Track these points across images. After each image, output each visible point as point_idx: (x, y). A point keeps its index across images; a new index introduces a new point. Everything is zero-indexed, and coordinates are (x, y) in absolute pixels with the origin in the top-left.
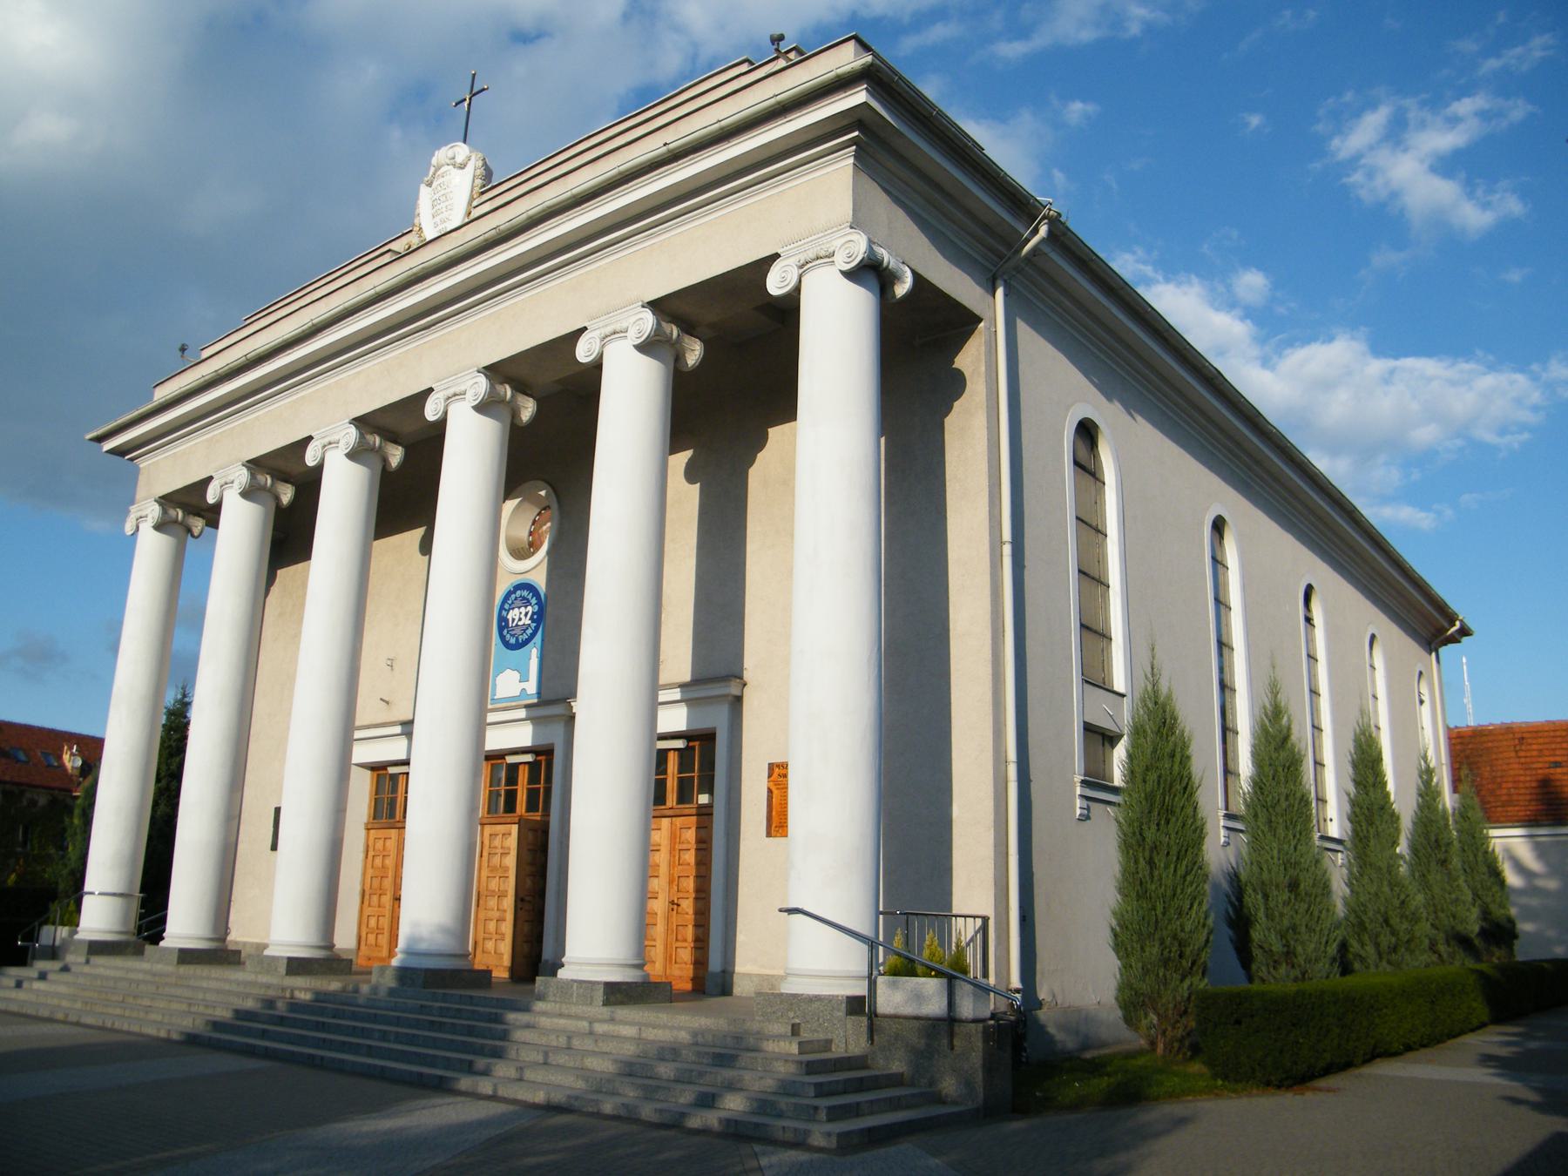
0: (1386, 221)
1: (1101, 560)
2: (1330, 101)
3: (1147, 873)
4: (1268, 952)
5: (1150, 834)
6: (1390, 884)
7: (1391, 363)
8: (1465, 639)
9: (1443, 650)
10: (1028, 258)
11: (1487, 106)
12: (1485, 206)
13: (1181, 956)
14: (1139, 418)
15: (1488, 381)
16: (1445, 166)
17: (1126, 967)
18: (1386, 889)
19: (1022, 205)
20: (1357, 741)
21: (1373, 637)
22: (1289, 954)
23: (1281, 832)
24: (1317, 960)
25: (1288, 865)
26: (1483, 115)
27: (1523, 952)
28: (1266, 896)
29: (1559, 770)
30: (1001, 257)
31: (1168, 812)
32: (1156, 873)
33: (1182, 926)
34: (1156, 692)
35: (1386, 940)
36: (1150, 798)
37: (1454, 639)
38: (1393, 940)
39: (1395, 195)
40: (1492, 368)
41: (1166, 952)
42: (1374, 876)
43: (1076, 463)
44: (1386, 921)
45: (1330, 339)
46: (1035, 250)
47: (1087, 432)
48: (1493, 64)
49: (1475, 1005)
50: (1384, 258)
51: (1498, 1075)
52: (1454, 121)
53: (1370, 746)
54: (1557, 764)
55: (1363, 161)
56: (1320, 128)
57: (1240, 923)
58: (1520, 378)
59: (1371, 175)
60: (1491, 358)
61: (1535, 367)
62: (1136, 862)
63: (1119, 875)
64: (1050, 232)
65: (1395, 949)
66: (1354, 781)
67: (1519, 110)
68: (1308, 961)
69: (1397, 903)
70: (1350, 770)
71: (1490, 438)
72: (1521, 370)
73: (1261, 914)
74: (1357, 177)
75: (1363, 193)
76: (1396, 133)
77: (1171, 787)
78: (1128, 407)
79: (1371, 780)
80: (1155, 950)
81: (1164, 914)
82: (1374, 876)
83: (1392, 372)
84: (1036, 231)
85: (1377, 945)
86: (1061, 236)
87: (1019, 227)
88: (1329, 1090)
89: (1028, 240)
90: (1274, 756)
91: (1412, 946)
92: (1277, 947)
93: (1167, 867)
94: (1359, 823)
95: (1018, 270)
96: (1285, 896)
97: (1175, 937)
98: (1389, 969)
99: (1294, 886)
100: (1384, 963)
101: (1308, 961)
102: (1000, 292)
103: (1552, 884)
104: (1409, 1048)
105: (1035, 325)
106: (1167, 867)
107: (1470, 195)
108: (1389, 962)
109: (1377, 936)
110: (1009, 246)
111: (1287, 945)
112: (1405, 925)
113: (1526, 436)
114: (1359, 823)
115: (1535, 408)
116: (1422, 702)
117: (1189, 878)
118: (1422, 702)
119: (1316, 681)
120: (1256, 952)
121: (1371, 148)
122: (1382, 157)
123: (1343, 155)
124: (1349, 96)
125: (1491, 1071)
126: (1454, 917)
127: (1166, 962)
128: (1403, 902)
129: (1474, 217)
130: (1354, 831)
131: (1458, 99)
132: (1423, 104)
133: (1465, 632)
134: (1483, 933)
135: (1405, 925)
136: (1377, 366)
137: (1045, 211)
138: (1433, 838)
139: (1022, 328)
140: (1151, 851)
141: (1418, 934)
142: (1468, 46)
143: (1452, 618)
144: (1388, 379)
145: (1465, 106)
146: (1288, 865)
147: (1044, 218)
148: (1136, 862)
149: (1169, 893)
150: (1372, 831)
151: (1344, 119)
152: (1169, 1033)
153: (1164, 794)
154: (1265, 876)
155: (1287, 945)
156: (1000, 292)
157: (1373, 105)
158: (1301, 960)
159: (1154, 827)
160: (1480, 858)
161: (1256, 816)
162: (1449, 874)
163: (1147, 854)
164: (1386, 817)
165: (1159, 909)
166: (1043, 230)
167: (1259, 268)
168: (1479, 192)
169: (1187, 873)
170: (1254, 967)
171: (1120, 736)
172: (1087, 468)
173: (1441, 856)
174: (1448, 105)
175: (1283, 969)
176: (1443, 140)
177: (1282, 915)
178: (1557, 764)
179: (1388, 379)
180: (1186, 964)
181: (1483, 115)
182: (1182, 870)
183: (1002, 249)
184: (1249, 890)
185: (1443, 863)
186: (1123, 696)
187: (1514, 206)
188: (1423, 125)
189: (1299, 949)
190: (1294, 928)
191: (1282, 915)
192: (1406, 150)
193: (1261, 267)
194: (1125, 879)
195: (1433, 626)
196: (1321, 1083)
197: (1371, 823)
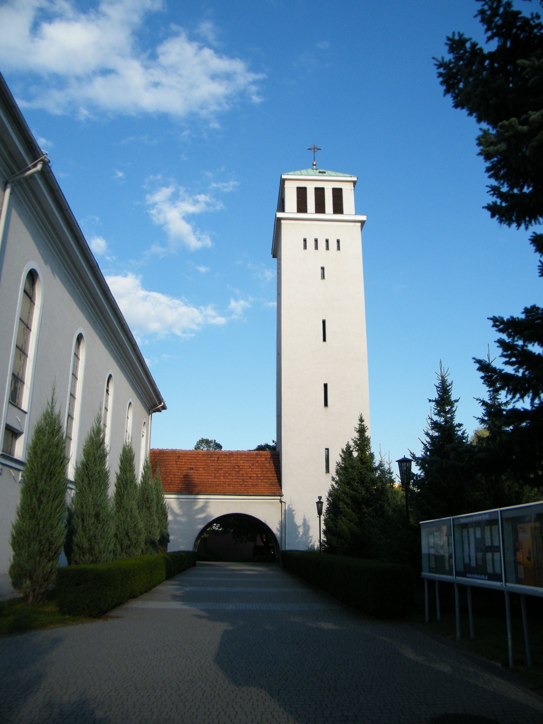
0: (160, 233)
1: (26, 342)
2: (151, 177)
3: (37, 505)
4: (80, 548)
5: (41, 485)
6: (131, 517)
7: (147, 293)
8: (163, 411)
9: (154, 414)
10: (26, 179)
11: (210, 201)
12: (199, 239)
13: (50, 550)
14: (56, 277)
15: (183, 309)
16: (189, 218)
17: (17, 555)
18: (129, 519)
19: (34, 151)
20: (124, 450)
21: (130, 403)
22: (91, 549)
23: (94, 489)
24: (104, 552)
25: (96, 505)
26: (207, 204)
27: (172, 548)
28: (83, 520)
29: (192, 471)
30: (13, 173)
31: (51, 474)
32: (42, 507)
33: (52, 534)
34: (52, 412)
35: (126, 542)
36: (43, 466)
37: (159, 410)
38: (129, 542)
39: (166, 223)
40: (186, 304)
41: (42, 548)
42: (124, 513)
43: (25, 291)
44: (127, 534)
45: (125, 276)
46: (32, 176)
47: (32, 276)
48: (214, 185)
49: (163, 572)
50: (156, 249)
51: (182, 604)
52: (196, 202)
53: (130, 452)
54: (192, 469)
55: (156, 206)
56: (145, 187)
57: (71, 532)
58: (196, 311)
59: (159, 213)
60: (187, 300)
61: (202, 307)
62: (31, 499)
63: (19, 506)
64: (42, 169)
65: (129, 547)
66: (120, 468)
67: (220, 206)
68: (100, 552)
69: (133, 525)
70: (119, 463)
71: (179, 333)
72: (198, 308)
73: (80, 529)
74: (154, 212)
75: (155, 219)
76: (174, 199)
77: (55, 461)
78: (53, 271)
79: (128, 468)
80: (36, 547)
81: (43, 528)
82: (124, 513)
83: (147, 296)
84: (35, 166)
85: (121, 545)
86: (46, 174)
87: (28, 161)
88: (118, 617)
89: (29, 169)
90: (95, 452)
91: (137, 545)
92: (86, 545)
93: (48, 503)
94: (120, 488)
95: (20, 183)
96: (92, 520)
97: (48, 540)
98: (125, 556)
99: (97, 516)
100: (124, 553)
101: (100, 552)
102: (8, 191)
103: (183, 519)
104: (141, 594)
105: (21, 215)
106: (48, 503)
107: (194, 233)
108: (126, 553)
109: (122, 540)
110: (19, 169)
111: (91, 544)
112: (135, 536)
113: (193, 335)
114: (120, 488)
115: (198, 325)
116: (143, 436)
117: (58, 509)
118: (143, 436)
119: (71, 430)
120: (75, 548)
121: (162, 202)
122: (165, 207)
123: (496, 39)
124: (159, 177)
125: (179, 603)
126: (150, 533)
127: (41, 553)
128: (135, 526)
129: (194, 243)
130: (117, 491)
131: (200, 194)
132: (186, 191)
133: (164, 408)
134: (160, 541)
135: (135, 536)
136: (142, 293)
137: (43, 157)
138: (146, 497)
139: (14, 213)
140: (40, 494)
141: (139, 540)
142: (209, 174)
143: (160, 400)
144: (145, 299)
145: (202, 198)
146: (96, 505)
147: (41, 160)
148: (31, 499)
149: (48, 516)
150: (126, 492)
151: (155, 187)
152: (37, 591)
153: (51, 465)
154: (84, 510)
155: (91, 544)
156: (8, 191)
157: (166, 185)
158: (96, 551)
159: (43, 482)
160: (159, 507)
161: (83, 481)
162: (151, 514)
163: (38, 495)
164: (133, 486)
165: (41, 526)
166: (39, 167)
167: (104, 238)
168: (197, 233)
169: (57, 507)
170: (72, 555)
171: (21, 433)
172: (29, 295)
173: (148, 505)
174: (196, 195)
175: (87, 556)
176: (189, 208)
177: (90, 530)
178: (192, 469)
179: (145, 299)
180: (51, 554)
181: (207, 204)
182: (55, 506)
183: (16, 170)
184: (75, 517)
185: (149, 508)
186: (26, 413)
187: (208, 242)
188: (184, 200)
189: (96, 547)
190: (95, 536)
191: (90, 530)
192: (176, 207)
193: (105, 237)
194: (22, 507)
195: (153, 402)
196: (113, 613)
197: (125, 488)
